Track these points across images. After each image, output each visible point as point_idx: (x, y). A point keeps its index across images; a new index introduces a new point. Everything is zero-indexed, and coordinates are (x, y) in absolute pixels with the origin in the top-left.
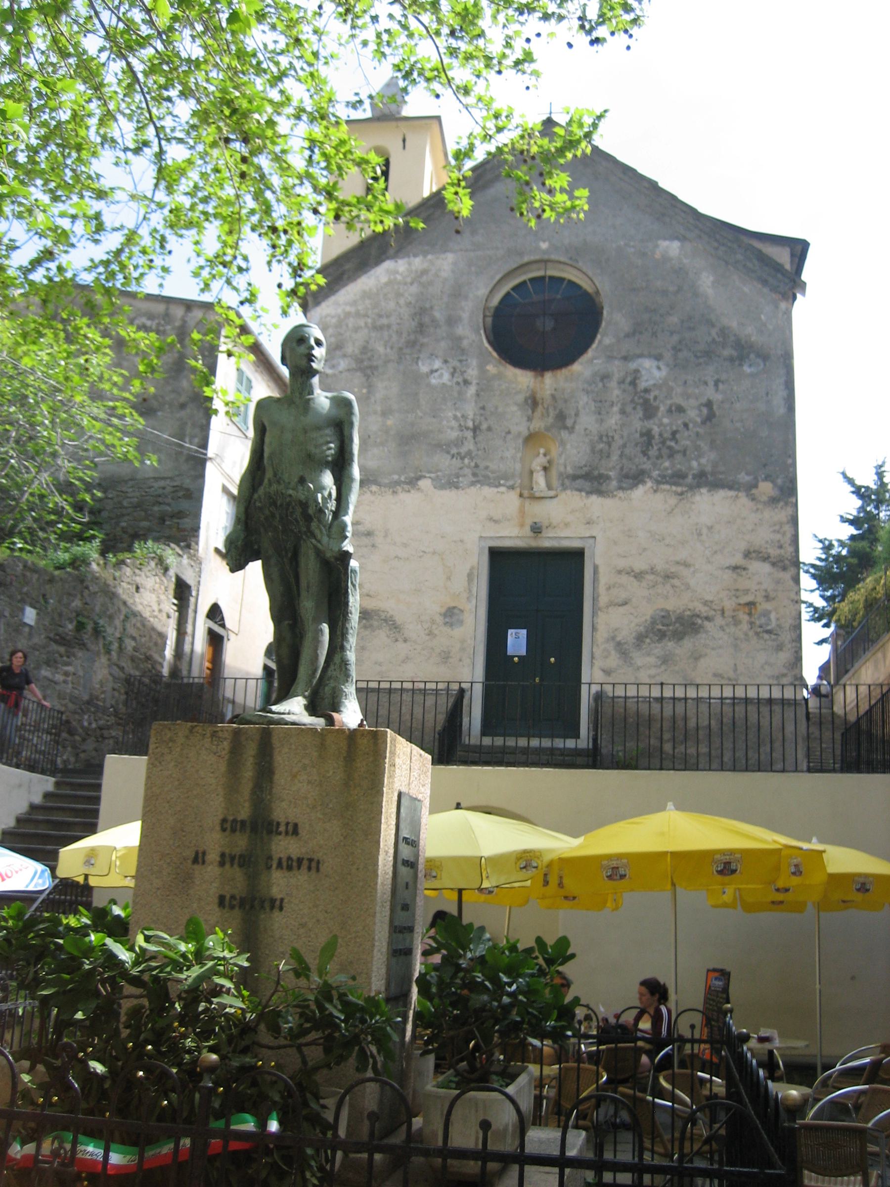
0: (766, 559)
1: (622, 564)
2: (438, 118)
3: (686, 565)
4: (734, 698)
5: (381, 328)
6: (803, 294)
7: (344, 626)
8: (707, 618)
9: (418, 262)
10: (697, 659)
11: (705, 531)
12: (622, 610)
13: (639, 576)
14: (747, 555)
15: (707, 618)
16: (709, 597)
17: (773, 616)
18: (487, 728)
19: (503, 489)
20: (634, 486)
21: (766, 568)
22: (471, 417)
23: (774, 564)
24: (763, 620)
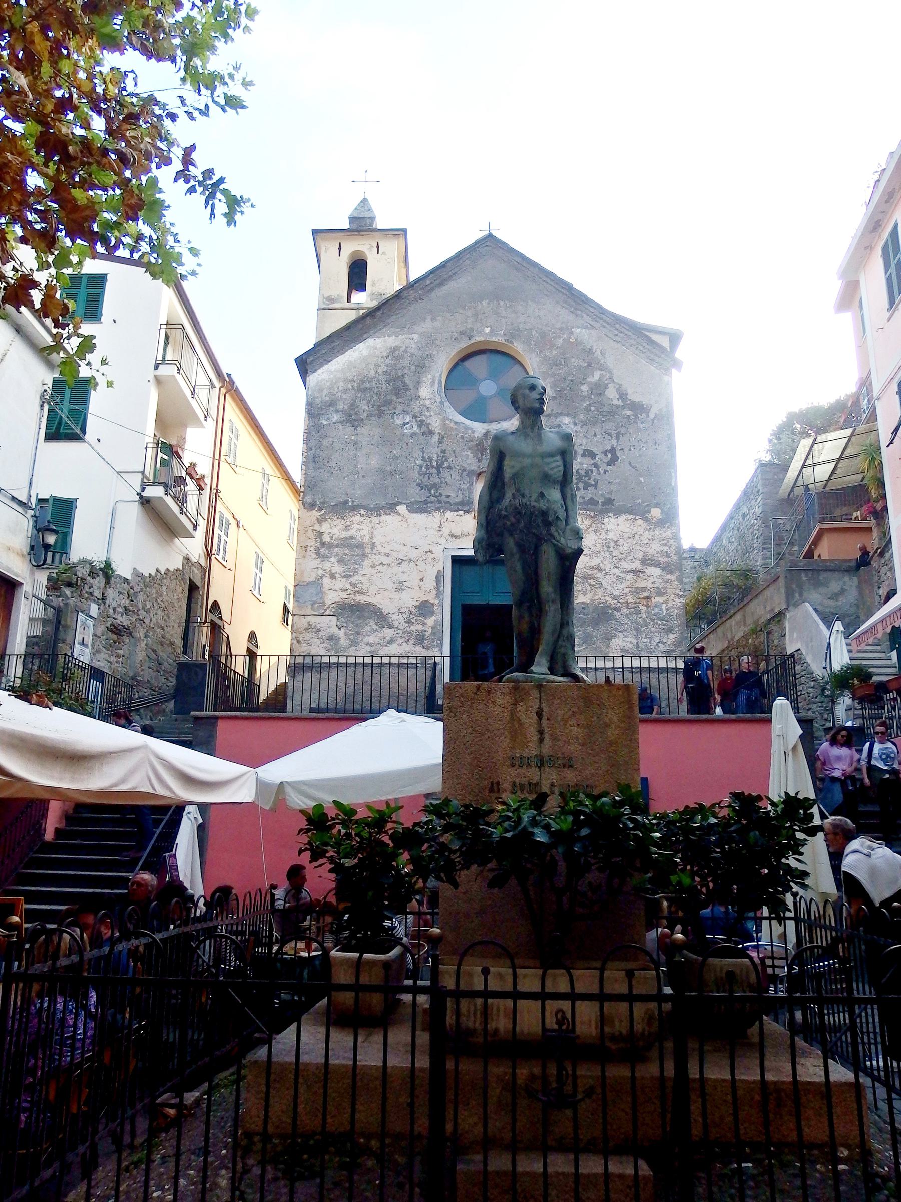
0: (657, 565)
2: (405, 231)
3: (600, 570)
4: (632, 668)
5: (365, 389)
6: (679, 369)
7: (568, 606)
10: (609, 639)
11: (612, 544)
14: (644, 562)
15: (616, 609)
16: (616, 593)
17: (664, 606)
19: (461, 513)
21: (657, 571)
22: (435, 458)
23: (663, 569)
24: (657, 610)
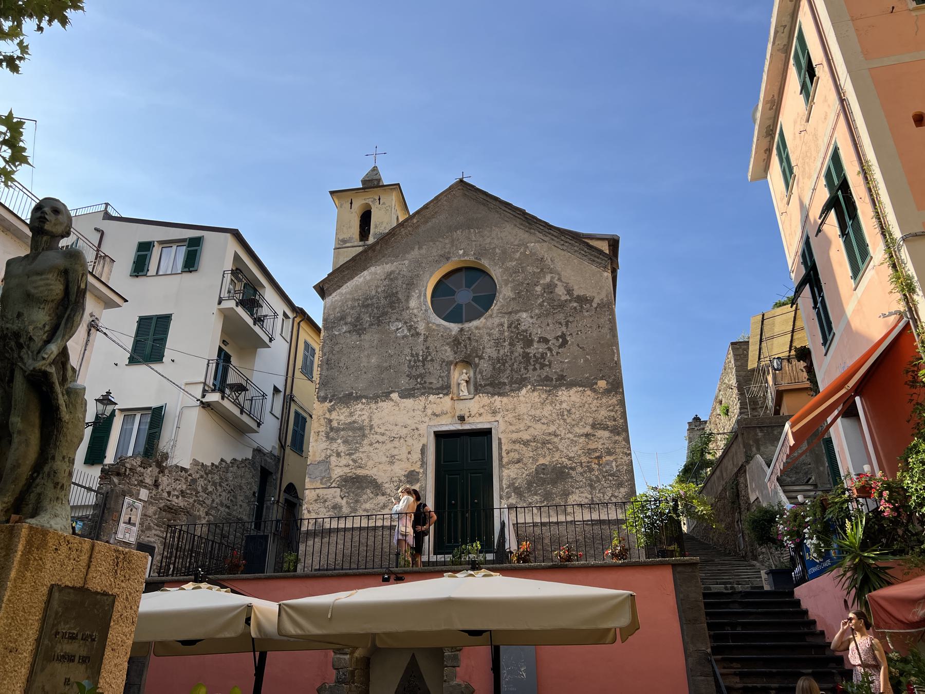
1: (515, 436)
2: (398, 184)
8: (573, 469)
9: (388, 267)
13: (526, 443)
14: (593, 426)
15: (573, 469)
20: (519, 389)
21: (606, 434)
23: (611, 431)
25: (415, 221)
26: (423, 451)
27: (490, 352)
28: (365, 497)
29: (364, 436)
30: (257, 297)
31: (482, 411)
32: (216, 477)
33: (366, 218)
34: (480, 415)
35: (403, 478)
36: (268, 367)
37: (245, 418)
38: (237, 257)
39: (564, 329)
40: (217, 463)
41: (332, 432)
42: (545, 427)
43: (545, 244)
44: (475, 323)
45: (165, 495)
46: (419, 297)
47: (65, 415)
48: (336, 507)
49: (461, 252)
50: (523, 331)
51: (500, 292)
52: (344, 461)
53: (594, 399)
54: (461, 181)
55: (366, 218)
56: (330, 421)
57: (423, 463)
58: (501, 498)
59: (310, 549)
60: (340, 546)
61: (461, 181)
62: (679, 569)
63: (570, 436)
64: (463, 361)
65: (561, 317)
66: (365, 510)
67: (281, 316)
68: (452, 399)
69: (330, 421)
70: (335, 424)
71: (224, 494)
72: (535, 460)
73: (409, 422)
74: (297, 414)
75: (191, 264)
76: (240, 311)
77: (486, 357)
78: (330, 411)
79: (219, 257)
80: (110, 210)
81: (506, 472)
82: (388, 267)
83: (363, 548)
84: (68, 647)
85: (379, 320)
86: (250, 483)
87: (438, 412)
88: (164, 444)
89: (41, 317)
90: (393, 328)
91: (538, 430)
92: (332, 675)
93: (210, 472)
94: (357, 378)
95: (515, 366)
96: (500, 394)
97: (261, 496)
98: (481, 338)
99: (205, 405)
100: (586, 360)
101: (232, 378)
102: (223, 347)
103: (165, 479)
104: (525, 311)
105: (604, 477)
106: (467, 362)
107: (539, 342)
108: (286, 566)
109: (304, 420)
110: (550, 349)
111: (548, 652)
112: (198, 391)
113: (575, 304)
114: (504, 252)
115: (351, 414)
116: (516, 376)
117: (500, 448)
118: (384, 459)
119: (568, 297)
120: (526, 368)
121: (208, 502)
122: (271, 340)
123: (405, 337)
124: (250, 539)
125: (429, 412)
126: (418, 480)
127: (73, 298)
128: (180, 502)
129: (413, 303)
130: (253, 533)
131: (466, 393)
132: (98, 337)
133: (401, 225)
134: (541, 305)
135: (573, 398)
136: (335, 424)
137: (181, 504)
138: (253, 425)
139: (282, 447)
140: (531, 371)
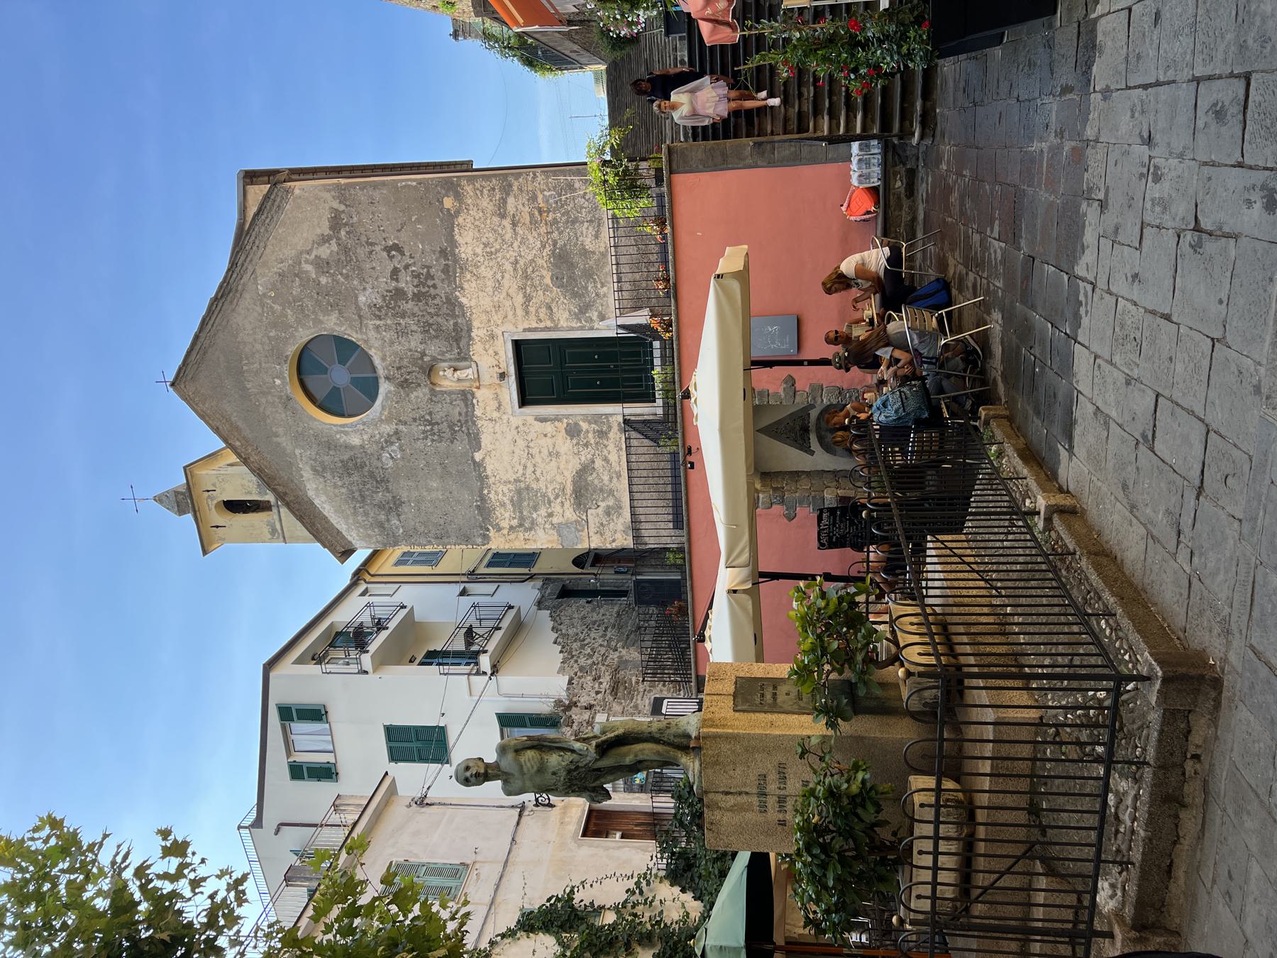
1: (520, 312)
2: (185, 468)
8: (555, 243)
9: (307, 474)
12: (555, 310)
13: (528, 299)
14: (503, 216)
15: (555, 243)
18: (649, 397)
20: (461, 305)
21: (511, 201)
23: (508, 194)
25: (238, 444)
26: (543, 420)
27: (415, 342)
28: (596, 482)
29: (528, 488)
30: (351, 630)
31: (491, 352)
32: (575, 645)
33: (234, 506)
34: (496, 354)
35: (575, 441)
36: (440, 608)
37: (505, 624)
38: (299, 661)
39: (378, 248)
40: (560, 648)
41: (524, 524)
42: (507, 275)
43: (259, 271)
44: (377, 361)
45: (600, 696)
46: (346, 433)
47: (621, 731)
48: (608, 513)
49: (278, 382)
50: (384, 300)
51: (333, 330)
52: (556, 508)
53: (469, 214)
54: (173, 385)
55: (234, 506)
56: (511, 528)
57: (558, 418)
58: (592, 329)
59: (654, 533)
60: (649, 503)
61: (173, 385)
62: (674, 166)
63: (516, 245)
64: (429, 376)
65: (362, 252)
66: (611, 480)
67: (366, 599)
68: (478, 388)
69: (511, 528)
70: (515, 522)
71: (592, 635)
72: (546, 289)
73: (509, 437)
74: (490, 565)
75: (316, 714)
76: (373, 648)
77: (422, 347)
78: (499, 529)
79: (300, 683)
80: (247, 823)
81: (563, 323)
82: (307, 474)
83: (651, 481)
84: (768, 697)
85: (382, 482)
86: (577, 608)
87: (495, 404)
88: (545, 708)
89: (554, 760)
90: (391, 463)
91: (511, 283)
92: (777, 509)
93: (570, 653)
94: (458, 502)
95: (432, 311)
96: (470, 330)
97: (590, 594)
98: (396, 354)
99: (495, 670)
100: (419, 221)
101: (459, 645)
102: (417, 661)
103: (582, 700)
104: (357, 297)
105: (562, 206)
106: (430, 371)
107: (397, 280)
108: (679, 562)
109: (496, 555)
110: (407, 267)
111: (755, 306)
112: (479, 681)
113: (343, 233)
114: (274, 325)
115: (503, 505)
116: (444, 310)
117: (535, 330)
118: (554, 464)
119: (333, 242)
120: (434, 298)
121: (603, 650)
122: (403, 607)
123: (401, 448)
124: (640, 601)
125: (495, 415)
126: (576, 424)
127: (536, 743)
128: (606, 680)
129: (355, 440)
130: (632, 599)
131: (470, 371)
132: (432, 796)
133: (245, 461)
134: (347, 277)
135: (469, 239)
136: (515, 522)
137: (608, 678)
138: (512, 613)
139: (532, 577)
140: (437, 291)
